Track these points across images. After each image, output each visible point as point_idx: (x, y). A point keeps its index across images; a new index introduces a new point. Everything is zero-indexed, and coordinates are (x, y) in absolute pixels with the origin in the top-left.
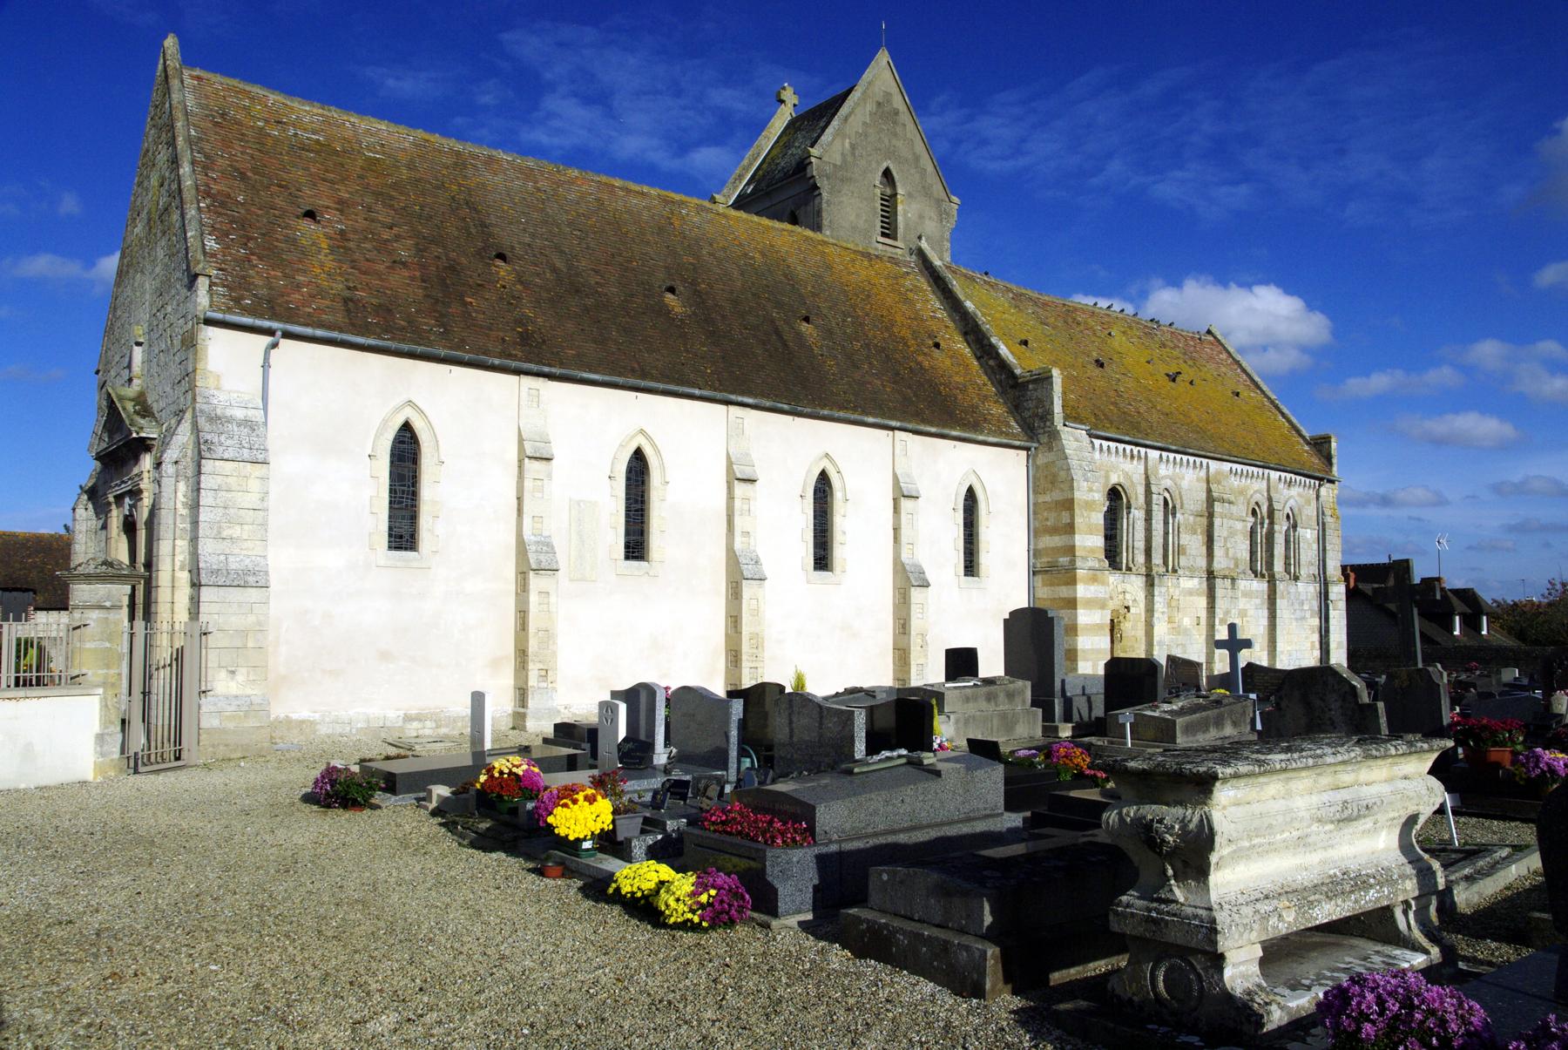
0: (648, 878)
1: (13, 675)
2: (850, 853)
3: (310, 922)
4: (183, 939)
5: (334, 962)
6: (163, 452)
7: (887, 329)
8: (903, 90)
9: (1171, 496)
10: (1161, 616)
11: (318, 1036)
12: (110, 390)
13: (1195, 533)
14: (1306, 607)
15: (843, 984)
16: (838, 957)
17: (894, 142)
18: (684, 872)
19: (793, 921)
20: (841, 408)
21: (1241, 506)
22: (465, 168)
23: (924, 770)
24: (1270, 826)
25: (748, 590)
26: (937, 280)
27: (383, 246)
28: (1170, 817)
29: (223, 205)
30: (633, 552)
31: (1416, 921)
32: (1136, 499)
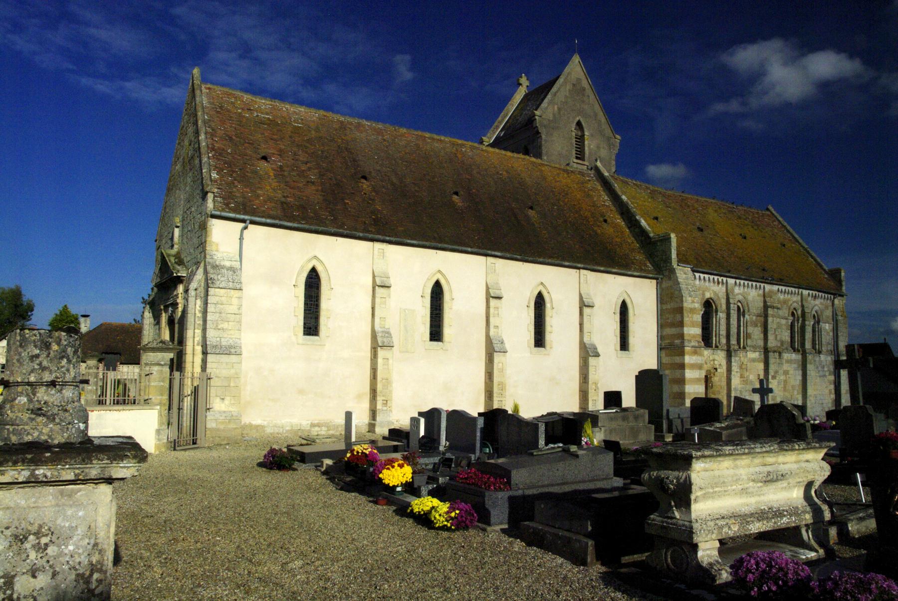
0: (427, 504)
2: (529, 496)
3: (262, 521)
4: (204, 526)
5: (273, 538)
6: (189, 284)
8: (588, 77)
9: (742, 305)
12: (163, 251)
13: (756, 326)
14: (826, 369)
15: (518, 557)
16: (518, 545)
19: (498, 528)
20: (551, 257)
22: (345, 129)
23: (572, 455)
24: (724, 482)
25: (497, 358)
26: (606, 184)
28: (672, 476)
29: (220, 154)
30: (434, 337)
32: (721, 306)
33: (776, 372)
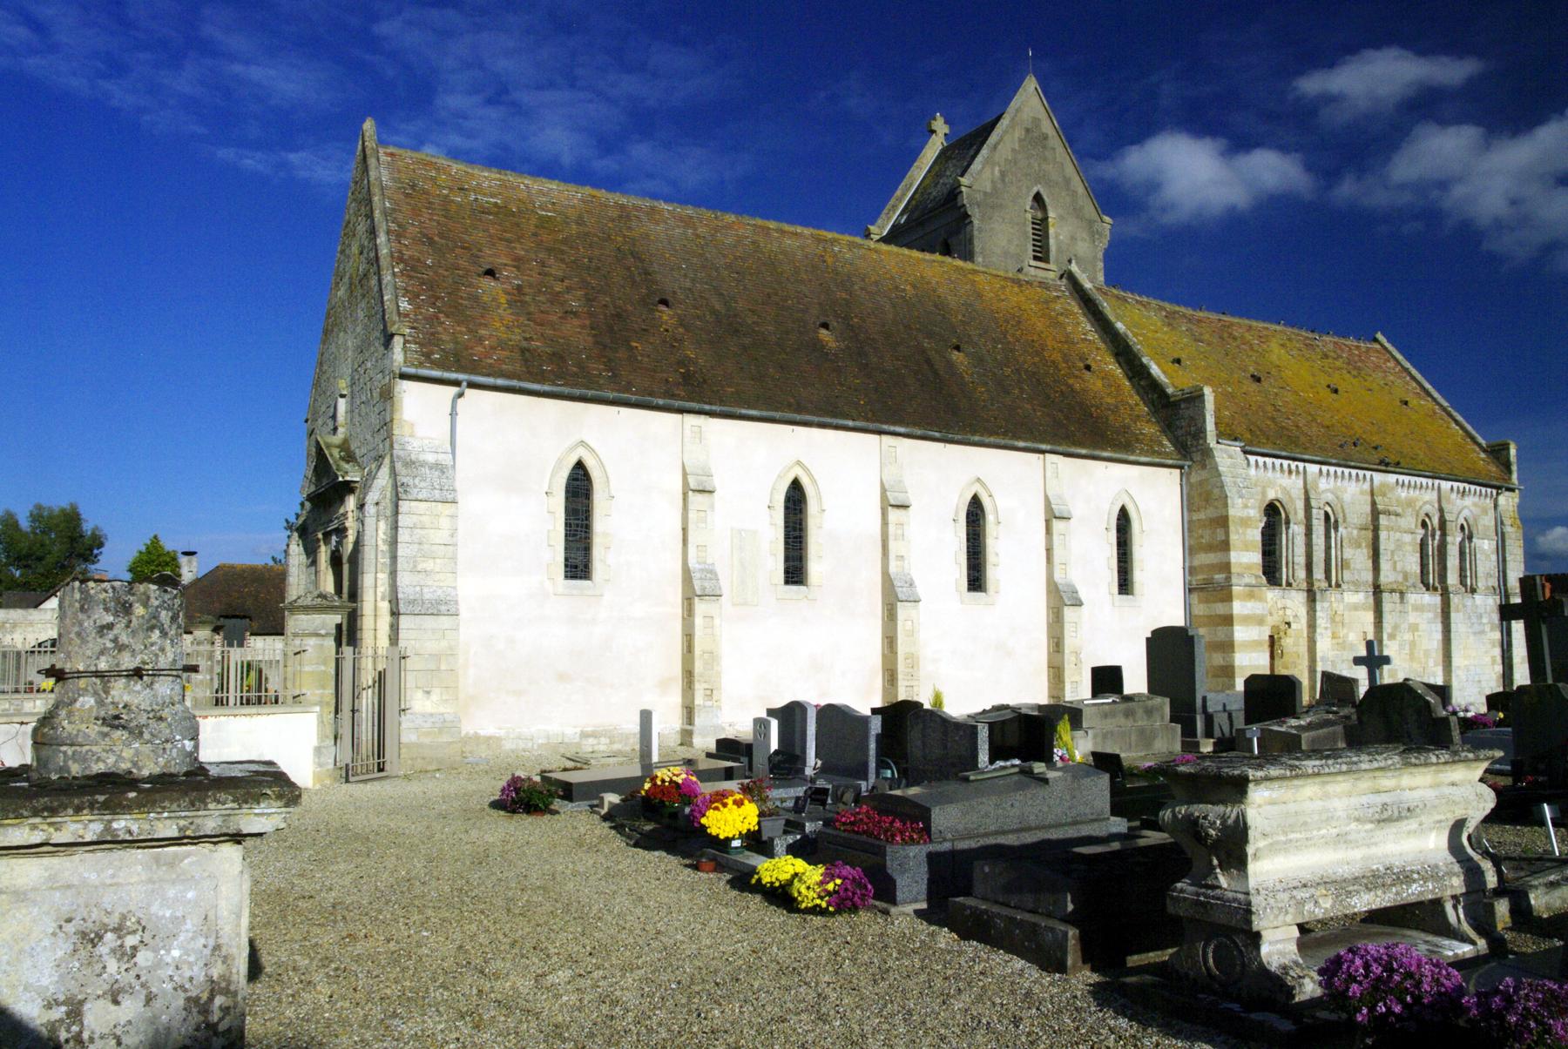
0: (786, 870)
1: (239, 695)
2: (963, 852)
3: (500, 902)
4: (400, 913)
5: (520, 932)
6: (365, 494)
7: (1038, 353)
9: (1333, 510)
10: (1323, 631)
11: (508, 984)
12: (319, 439)
13: (1359, 546)
14: (1485, 620)
15: (944, 960)
16: (945, 938)
17: (1044, 166)
18: (815, 864)
19: (910, 909)
20: (991, 434)
21: (1409, 518)
22: (630, 220)
23: (1034, 778)
24: (1305, 823)
25: (903, 611)
27: (555, 298)
28: (1213, 814)
29: (413, 269)
31: (1465, 915)
32: (1296, 513)
33: (1396, 627)
